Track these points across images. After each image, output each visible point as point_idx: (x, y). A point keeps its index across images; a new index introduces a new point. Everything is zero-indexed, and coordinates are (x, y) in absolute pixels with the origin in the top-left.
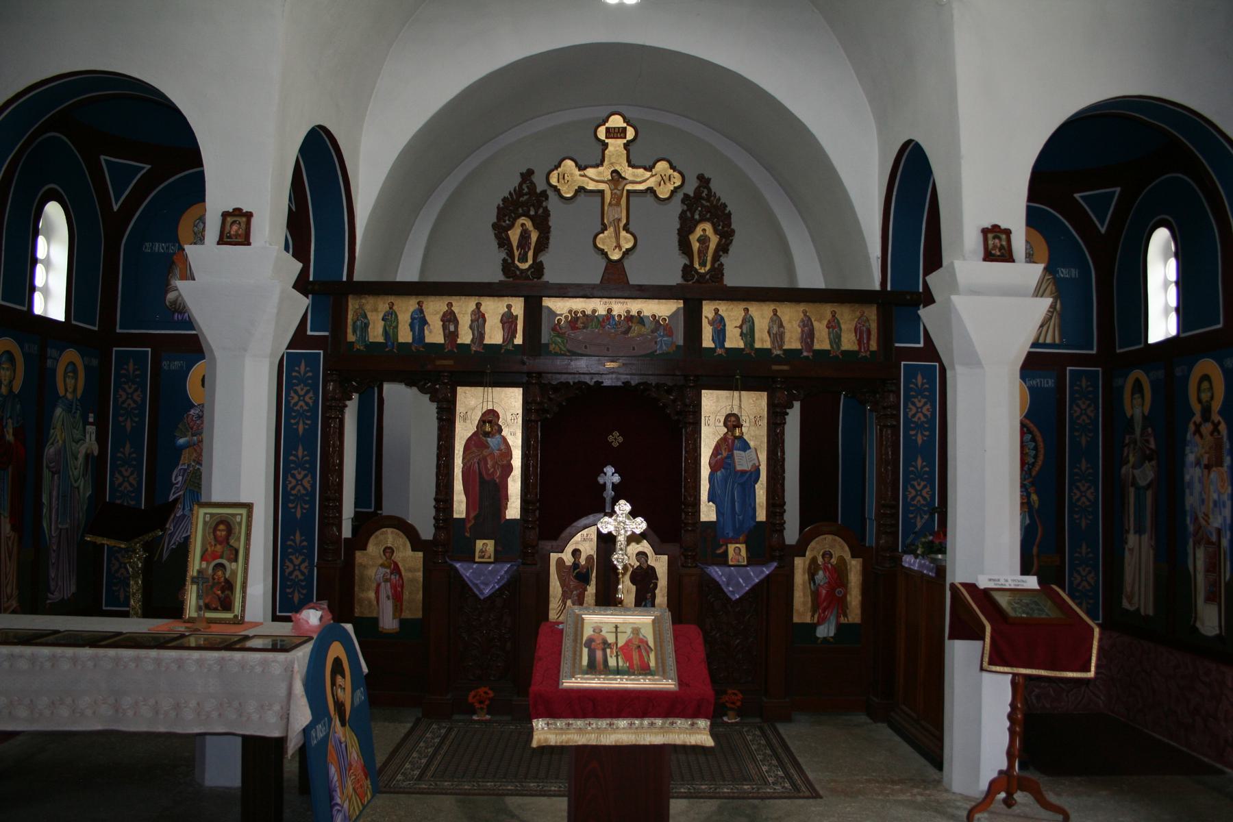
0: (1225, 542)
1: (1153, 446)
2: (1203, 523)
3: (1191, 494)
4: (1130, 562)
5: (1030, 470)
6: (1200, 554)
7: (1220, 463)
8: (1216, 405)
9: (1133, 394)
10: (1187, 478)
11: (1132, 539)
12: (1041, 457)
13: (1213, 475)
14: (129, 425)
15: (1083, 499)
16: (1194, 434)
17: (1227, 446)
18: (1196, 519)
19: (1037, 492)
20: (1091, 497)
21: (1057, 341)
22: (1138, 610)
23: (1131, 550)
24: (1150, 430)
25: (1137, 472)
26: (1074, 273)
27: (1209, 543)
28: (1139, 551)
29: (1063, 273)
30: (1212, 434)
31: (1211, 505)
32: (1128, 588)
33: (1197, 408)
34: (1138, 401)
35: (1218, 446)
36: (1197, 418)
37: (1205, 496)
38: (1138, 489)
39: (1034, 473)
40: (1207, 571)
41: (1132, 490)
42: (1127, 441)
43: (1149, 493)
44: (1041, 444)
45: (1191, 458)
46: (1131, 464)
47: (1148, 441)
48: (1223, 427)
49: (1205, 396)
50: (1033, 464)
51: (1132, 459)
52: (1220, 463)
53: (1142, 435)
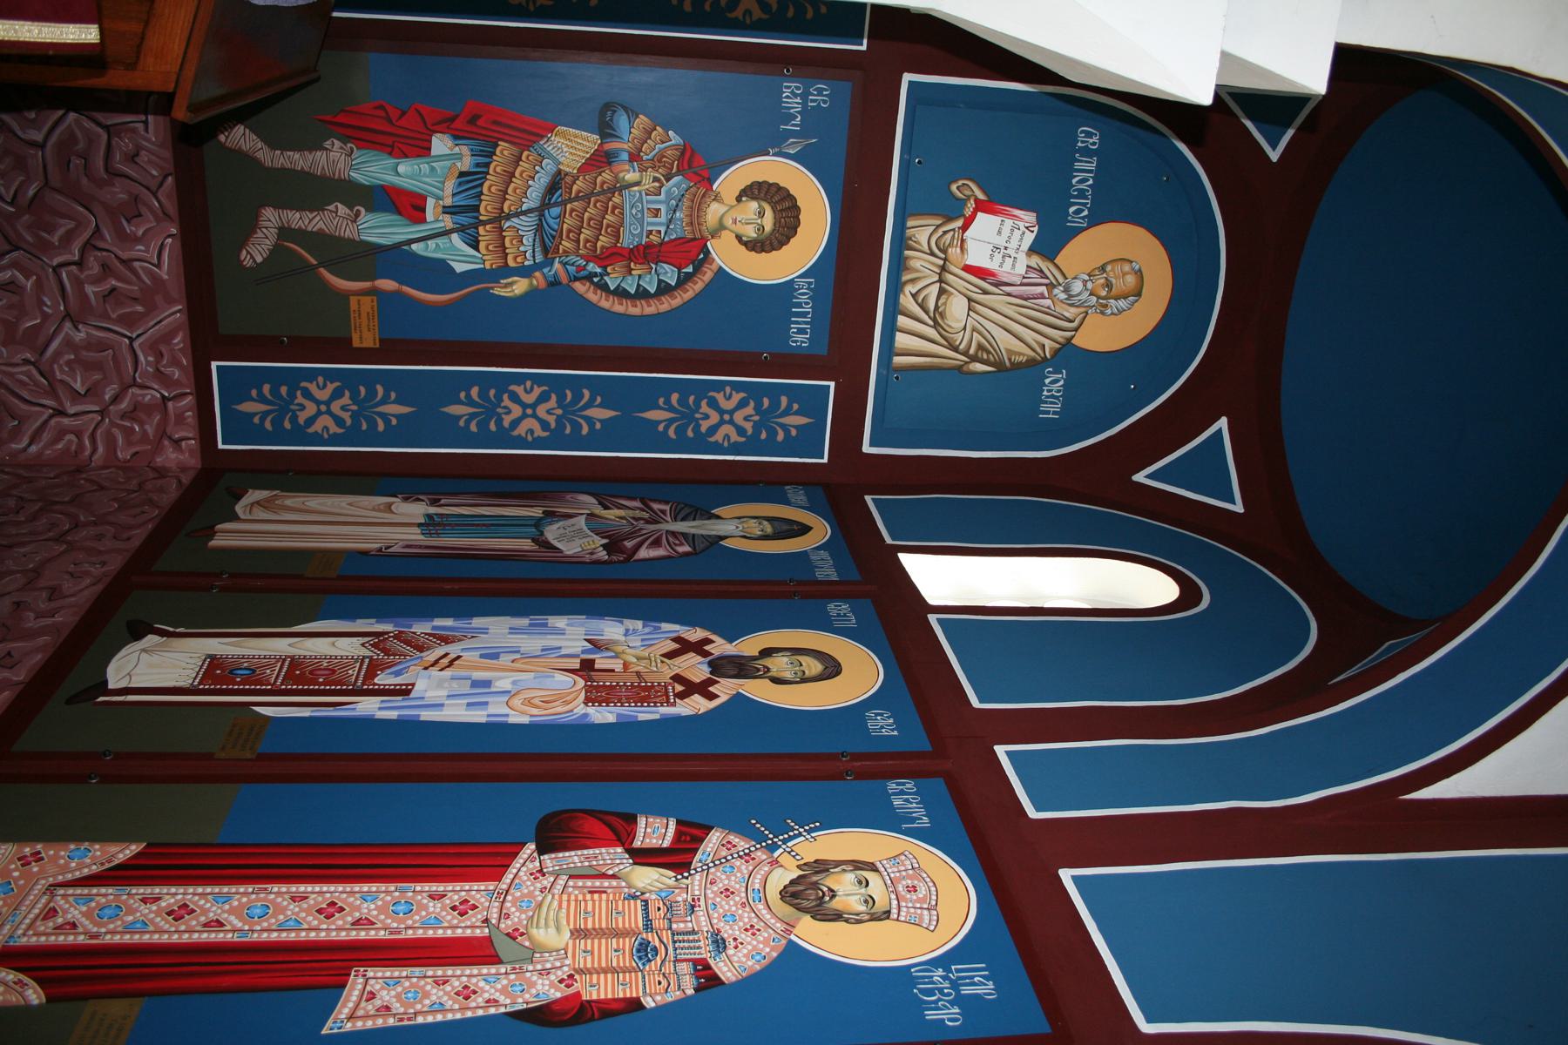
0: (368, 706)
1: (644, 553)
2: (431, 656)
3: (514, 630)
4: (366, 505)
5: (589, 277)
6: (349, 648)
7: (596, 696)
8: (758, 690)
9: (769, 519)
10: (560, 622)
11: (417, 510)
12: (619, 307)
13: (564, 680)
14: (600, 414)
15: (517, 411)
16: (677, 640)
17: (646, 714)
18: (446, 640)
19: (531, 293)
20: (521, 430)
21: (897, 360)
22: (235, 517)
23: (389, 507)
24: (686, 548)
25: (581, 522)
26: (1051, 410)
27: (374, 668)
28: (393, 524)
29: (1054, 383)
30: (677, 678)
31: (478, 675)
32: (293, 500)
33: (749, 646)
34: (755, 528)
35: (644, 693)
36: (720, 647)
37: (505, 659)
38: (538, 523)
39: (578, 286)
40: (295, 662)
41: (537, 512)
42: (656, 506)
43: (526, 544)
44: (650, 308)
45: (612, 630)
46: (599, 511)
47: (657, 543)
48: (697, 705)
49: (780, 665)
50: (604, 287)
51: (612, 514)
52: (596, 696)
53: (674, 534)
